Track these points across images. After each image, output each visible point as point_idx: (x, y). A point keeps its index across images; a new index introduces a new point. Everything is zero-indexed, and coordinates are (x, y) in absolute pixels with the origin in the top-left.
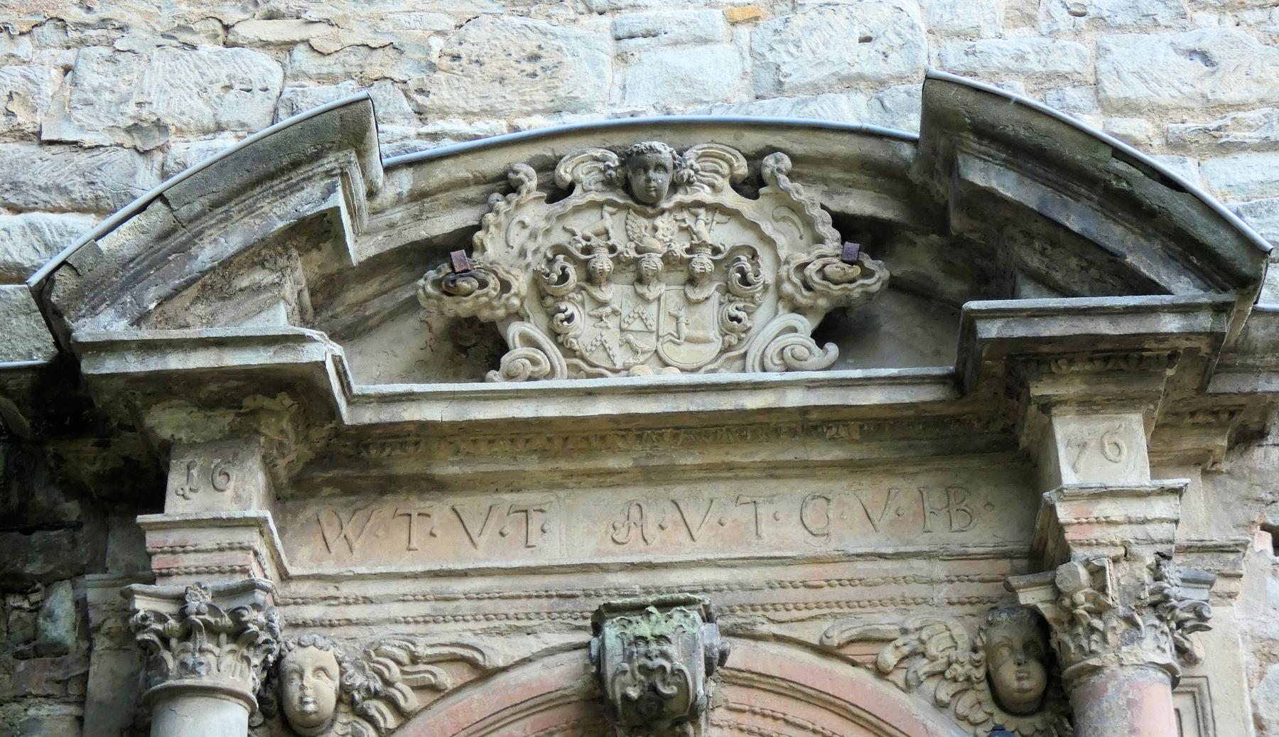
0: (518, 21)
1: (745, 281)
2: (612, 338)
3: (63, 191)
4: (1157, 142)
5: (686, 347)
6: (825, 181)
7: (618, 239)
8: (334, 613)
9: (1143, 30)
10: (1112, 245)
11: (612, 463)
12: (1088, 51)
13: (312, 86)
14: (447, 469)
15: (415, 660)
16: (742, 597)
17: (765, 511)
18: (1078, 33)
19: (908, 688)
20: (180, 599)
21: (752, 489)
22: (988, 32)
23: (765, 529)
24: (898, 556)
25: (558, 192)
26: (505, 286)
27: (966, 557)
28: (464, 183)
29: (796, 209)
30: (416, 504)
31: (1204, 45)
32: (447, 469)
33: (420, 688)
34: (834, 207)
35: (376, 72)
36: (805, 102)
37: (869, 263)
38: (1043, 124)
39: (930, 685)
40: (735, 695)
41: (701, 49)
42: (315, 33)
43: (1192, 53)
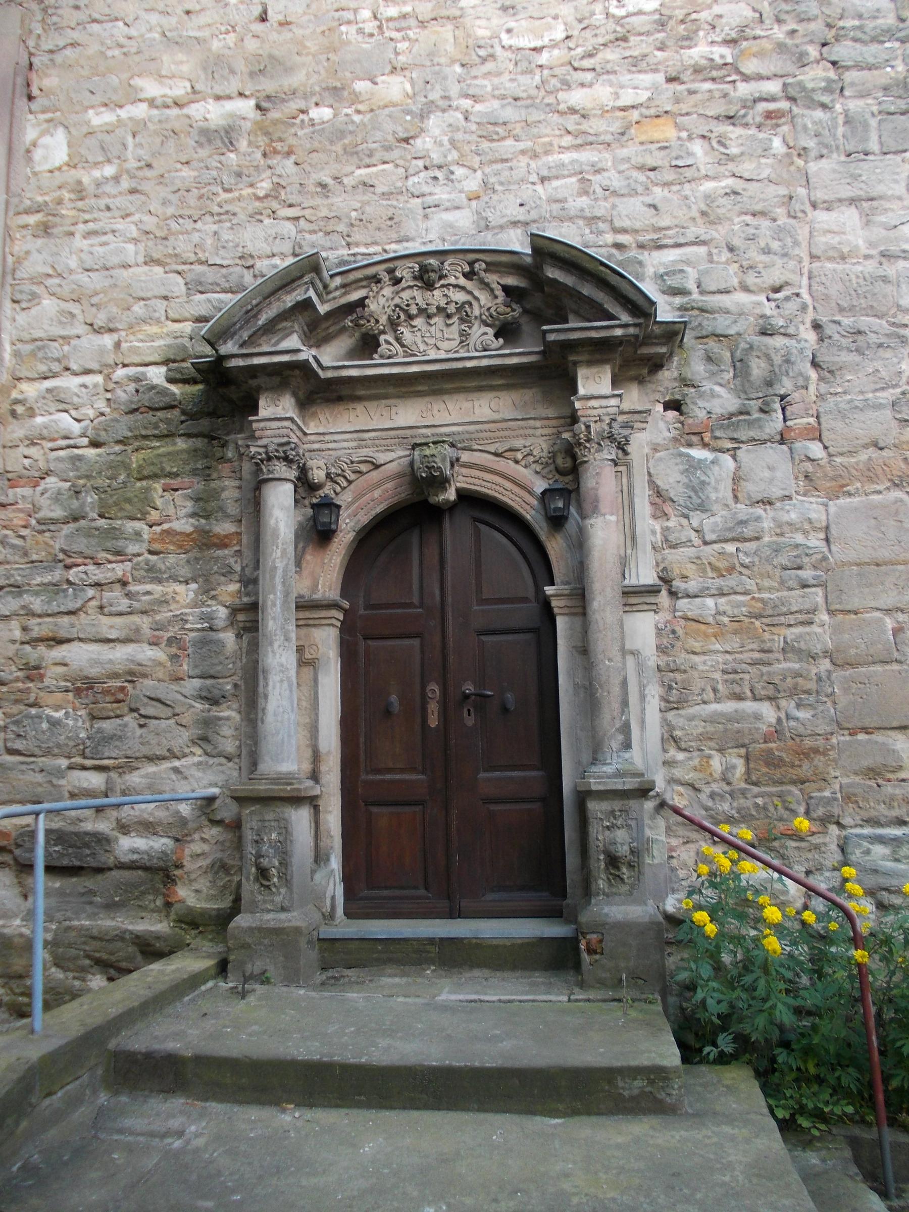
0: (385, 202)
1: (467, 315)
2: (419, 340)
3: (218, 285)
4: (634, 245)
5: (447, 342)
6: (499, 272)
7: (419, 300)
8: (324, 446)
9: (630, 195)
10: (598, 300)
11: (420, 388)
12: (608, 205)
13: (307, 236)
14: (361, 393)
15: (352, 462)
16: (467, 436)
17: (476, 403)
18: (606, 199)
19: (526, 467)
20: (265, 447)
21: (472, 396)
22: (570, 200)
23: (476, 411)
24: (523, 419)
25: (397, 281)
26: (377, 321)
27: (548, 418)
28: (361, 280)
29: (487, 285)
30: (351, 405)
31: (656, 202)
32: (361, 393)
33: (354, 472)
34: (502, 282)
35: (329, 229)
36: (497, 234)
37: (514, 306)
38: (574, 252)
39: (534, 466)
40: (464, 471)
41: (457, 212)
42: (307, 213)
43: (650, 206)
